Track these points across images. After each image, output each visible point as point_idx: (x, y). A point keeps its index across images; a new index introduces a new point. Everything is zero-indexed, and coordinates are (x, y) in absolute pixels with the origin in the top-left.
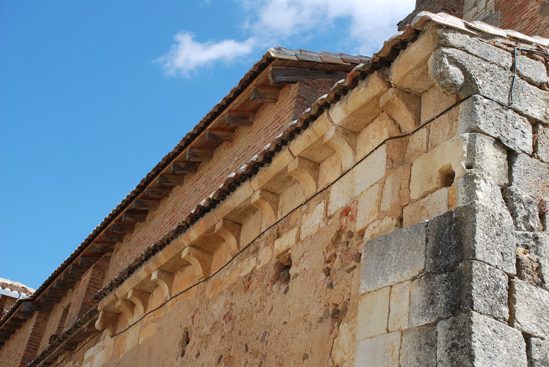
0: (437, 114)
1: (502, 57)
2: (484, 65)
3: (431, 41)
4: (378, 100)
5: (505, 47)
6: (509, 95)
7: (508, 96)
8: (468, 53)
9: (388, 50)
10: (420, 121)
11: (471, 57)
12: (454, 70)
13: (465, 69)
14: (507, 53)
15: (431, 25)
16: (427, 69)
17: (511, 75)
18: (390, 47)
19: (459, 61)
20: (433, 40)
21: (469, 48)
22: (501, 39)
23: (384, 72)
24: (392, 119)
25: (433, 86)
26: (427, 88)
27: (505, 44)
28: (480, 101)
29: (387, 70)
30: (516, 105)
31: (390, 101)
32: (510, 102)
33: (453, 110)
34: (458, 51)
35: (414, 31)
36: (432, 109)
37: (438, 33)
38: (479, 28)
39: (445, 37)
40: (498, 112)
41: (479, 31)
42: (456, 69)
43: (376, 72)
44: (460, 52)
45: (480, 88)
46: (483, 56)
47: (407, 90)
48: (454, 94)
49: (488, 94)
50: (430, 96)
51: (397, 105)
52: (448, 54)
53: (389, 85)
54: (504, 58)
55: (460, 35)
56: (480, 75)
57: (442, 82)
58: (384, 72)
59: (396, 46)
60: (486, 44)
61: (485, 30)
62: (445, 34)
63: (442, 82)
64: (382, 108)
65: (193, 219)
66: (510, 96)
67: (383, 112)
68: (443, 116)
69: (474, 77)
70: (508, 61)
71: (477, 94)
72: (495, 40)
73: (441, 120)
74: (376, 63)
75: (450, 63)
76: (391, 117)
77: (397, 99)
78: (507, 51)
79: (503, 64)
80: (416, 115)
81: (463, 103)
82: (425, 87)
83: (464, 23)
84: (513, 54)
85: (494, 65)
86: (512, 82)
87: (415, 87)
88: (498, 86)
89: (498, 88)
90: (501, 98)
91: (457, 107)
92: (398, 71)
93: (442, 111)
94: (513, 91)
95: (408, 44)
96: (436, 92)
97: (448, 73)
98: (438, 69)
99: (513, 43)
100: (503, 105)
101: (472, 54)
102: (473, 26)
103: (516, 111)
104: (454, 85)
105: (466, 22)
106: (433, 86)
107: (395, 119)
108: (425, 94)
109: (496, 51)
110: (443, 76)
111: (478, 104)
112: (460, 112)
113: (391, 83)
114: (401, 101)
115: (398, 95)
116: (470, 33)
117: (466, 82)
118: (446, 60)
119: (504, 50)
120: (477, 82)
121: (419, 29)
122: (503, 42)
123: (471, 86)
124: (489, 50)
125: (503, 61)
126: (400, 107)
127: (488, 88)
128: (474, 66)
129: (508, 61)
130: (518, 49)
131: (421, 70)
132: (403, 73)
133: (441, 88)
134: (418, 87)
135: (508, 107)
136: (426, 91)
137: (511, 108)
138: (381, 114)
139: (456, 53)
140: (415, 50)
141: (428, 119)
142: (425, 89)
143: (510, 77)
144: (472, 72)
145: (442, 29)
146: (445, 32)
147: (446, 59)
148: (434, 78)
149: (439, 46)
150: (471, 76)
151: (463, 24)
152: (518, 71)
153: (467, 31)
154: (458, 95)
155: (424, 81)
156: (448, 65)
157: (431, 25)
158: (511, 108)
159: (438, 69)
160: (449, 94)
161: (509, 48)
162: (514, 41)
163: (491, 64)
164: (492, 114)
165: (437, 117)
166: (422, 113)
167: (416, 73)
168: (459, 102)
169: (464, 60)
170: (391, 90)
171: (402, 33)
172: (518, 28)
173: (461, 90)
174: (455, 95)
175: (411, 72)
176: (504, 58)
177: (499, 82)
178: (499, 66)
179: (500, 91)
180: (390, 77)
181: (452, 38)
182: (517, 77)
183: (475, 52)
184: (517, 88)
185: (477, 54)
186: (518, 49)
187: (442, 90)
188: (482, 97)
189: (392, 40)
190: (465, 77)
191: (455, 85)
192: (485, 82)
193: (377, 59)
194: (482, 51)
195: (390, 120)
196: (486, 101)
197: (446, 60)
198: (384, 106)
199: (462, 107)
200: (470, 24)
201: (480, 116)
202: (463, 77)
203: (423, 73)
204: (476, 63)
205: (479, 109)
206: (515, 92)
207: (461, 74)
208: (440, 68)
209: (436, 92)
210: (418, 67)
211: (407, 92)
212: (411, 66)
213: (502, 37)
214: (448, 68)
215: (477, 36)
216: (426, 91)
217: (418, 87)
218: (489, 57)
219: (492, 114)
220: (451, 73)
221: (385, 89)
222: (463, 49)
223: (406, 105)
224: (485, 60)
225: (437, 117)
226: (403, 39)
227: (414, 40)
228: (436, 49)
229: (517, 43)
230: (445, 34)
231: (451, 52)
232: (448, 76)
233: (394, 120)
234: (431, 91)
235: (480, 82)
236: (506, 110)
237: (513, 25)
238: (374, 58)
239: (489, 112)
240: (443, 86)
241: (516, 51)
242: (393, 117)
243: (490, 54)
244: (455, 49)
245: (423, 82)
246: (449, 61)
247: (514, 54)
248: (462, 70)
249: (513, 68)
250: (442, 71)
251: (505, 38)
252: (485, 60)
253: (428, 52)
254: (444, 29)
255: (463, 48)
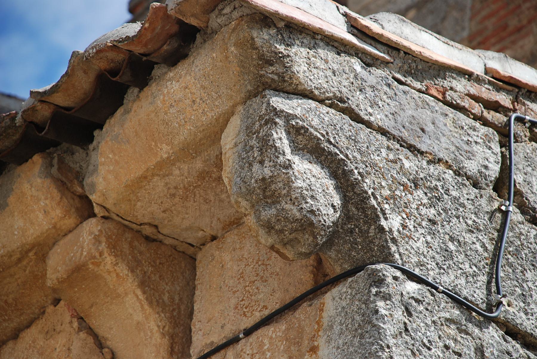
0: (248, 323)
1: (468, 143)
2: (407, 164)
3: (235, 68)
4: (42, 258)
5: (477, 108)
6: (490, 275)
7: (485, 278)
8: (356, 118)
9: (85, 83)
10: (189, 341)
11: (364, 133)
12: (307, 174)
13: (347, 174)
14: (484, 130)
15: (236, 14)
16: (219, 165)
17: (496, 205)
18: (92, 76)
19: (325, 145)
20: (241, 64)
21: (359, 101)
22: (464, 81)
23: (68, 159)
24: (91, 332)
25: (236, 222)
26: (215, 228)
27: (477, 99)
28: (391, 286)
29: (79, 153)
30: (512, 310)
31: (84, 265)
32: (494, 298)
33: (303, 313)
34: (324, 109)
35: (175, 29)
36: (233, 301)
37: (258, 42)
38: (394, 38)
39: (280, 58)
40: (452, 331)
41: (392, 47)
42: (316, 169)
43: (37, 159)
44: (128, 223)
45: (394, 241)
46: (405, 134)
47: (148, 231)
48: (307, 255)
49: (420, 264)
50: (226, 257)
51: (111, 279)
52: (288, 117)
53: (85, 209)
54: (475, 148)
55: (331, 55)
56: (393, 197)
57: (269, 213)
58: (68, 159)
59: (114, 72)
60: (416, 94)
61: (414, 48)
62: (281, 48)
63: (269, 213)
64: (54, 290)
65: (129, 221)
66: (493, 277)
67: (56, 302)
68: (270, 331)
69: (373, 202)
70: (486, 158)
71: (384, 261)
72: (446, 84)
73: (262, 345)
74: (39, 127)
75: (296, 149)
76: (84, 324)
77: (109, 259)
78: (486, 123)
79: (472, 167)
80: (174, 321)
81: (335, 291)
82: (209, 225)
83: (345, 15)
84: (505, 135)
85: (441, 168)
86: (501, 231)
87: (177, 220)
88: (452, 239)
89: (452, 247)
90: (463, 281)
91: (316, 302)
92: (116, 161)
93: (267, 312)
94: (502, 262)
95: (157, 72)
96: (249, 246)
97: (288, 183)
98: (256, 167)
99: (505, 99)
100: (469, 309)
101: (368, 124)
102: (375, 28)
103: (512, 331)
104: (307, 224)
105: (354, 15)
106: (236, 222)
107: (101, 332)
108: (211, 247)
109: (449, 122)
110: (272, 191)
111: (387, 297)
112: (325, 321)
113: (89, 203)
114: (123, 269)
115: (113, 247)
116: (365, 52)
117: (347, 216)
118: (281, 139)
119: (476, 118)
120: (383, 223)
121: (193, 22)
122: (473, 91)
123: (364, 234)
124: (425, 116)
125: (470, 156)
126: (121, 290)
127: (420, 244)
128: (378, 166)
129: (486, 158)
130: (520, 120)
131: (199, 165)
132: (137, 170)
133: (262, 232)
134: (186, 224)
135: (486, 314)
136: (214, 238)
137: (496, 321)
138: (50, 309)
139: (318, 118)
140: (180, 95)
141: (217, 339)
142: (209, 232)
143: (492, 214)
144: (367, 185)
145: (273, 31)
146: (282, 41)
147: (284, 135)
148: (240, 194)
149: (262, 87)
150: (363, 198)
151: (342, 19)
152: (518, 193)
153: (353, 46)
154: (319, 262)
155: (207, 201)
156: (289, 156)
157: (236, 14)
158: (496, 321)
159: (256, 167)
160: (290, 256)
161: (490, 115)
162: (508, 92)
163: (429, 162)
164: (433, 335)
165: (248, 332)
166: (197, 315)
167: (183, 173)
168: (322, 284)
169: (343, 142)
170: (92, 226)
171: (137, 27)
172: (528, 44)
173: (330, 243)
174: (311, 261)
175: (163, 167)
176: (475, 148)
177: (458, 227)
178: (457, 173)
179: (461, 258)
180: (87, 181)
181: (306, 64)
182: (515, 216)
183: (378, 118)
184: (516, 254)
185: (387, 124)
186: (520, 120)
187: (266, 240)
188: (398, 274)
189: (100, 50)
190: (346, 200)
191: (312, 224)
192: (410, 224)
193: (45, 112)
194: (404, 117)
195: (83, 335)
196: (411, 287)
197: (281, 139)
198: (61, 281)
199: (333, 301)
200: (365, 21)
201: (392, 342)
202: (337, 200)
203: (202, 175)
204: (381, 157)
205: (390, 316)
206: (511, 265)
207: (331, 190)
208: (262, 162)
209: (249, 246)
210: (188, 151)
211: (147, 238)
212: (165, 147)
213: (468, 75)
214: (288, 166)
215: (386, 63)
216: (214, 238)
217: (187, 221)
218: (425, 138)
219: (433, 335)
220: (299, 183)
221: (70, 222)
222: (339, 103)
223: (143, 284)
224: (412, 148)
225: (248, 332)
226: (138, 50)
227: (175, 59)
228: (252, 95)
229: (516, 100)
230: (281, 48)
231: (298, 112)
232: (288, 194)
233: (95, 336)
234: (231, 238)
235: (393, 222)
236: (480, 326)
237: (512, 34)
238: (32, 109)
239: (423, 327)
240: (269, 227)
241: (515, 128)
242: (94, 323)
243: (430, 128)
244: (313, 104)
245: (205, 207)
246: (292, 142)
247: (509, 136)
248: (334, 175)
249: (503, 184)
250: (267, 172)
251: (478, 80)
252: (412, 148)
253: (226, 106)
254: (279, 30)
255: (342, 100)
